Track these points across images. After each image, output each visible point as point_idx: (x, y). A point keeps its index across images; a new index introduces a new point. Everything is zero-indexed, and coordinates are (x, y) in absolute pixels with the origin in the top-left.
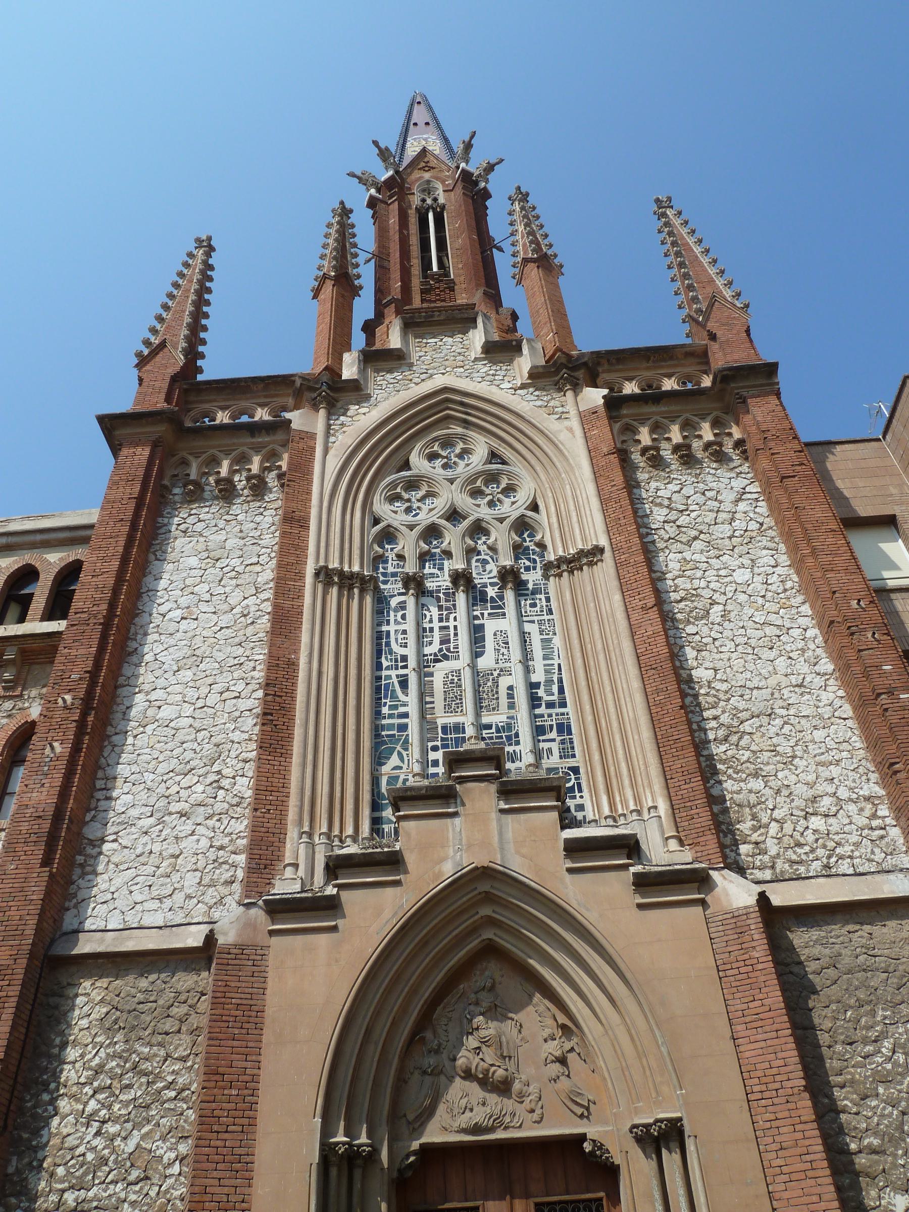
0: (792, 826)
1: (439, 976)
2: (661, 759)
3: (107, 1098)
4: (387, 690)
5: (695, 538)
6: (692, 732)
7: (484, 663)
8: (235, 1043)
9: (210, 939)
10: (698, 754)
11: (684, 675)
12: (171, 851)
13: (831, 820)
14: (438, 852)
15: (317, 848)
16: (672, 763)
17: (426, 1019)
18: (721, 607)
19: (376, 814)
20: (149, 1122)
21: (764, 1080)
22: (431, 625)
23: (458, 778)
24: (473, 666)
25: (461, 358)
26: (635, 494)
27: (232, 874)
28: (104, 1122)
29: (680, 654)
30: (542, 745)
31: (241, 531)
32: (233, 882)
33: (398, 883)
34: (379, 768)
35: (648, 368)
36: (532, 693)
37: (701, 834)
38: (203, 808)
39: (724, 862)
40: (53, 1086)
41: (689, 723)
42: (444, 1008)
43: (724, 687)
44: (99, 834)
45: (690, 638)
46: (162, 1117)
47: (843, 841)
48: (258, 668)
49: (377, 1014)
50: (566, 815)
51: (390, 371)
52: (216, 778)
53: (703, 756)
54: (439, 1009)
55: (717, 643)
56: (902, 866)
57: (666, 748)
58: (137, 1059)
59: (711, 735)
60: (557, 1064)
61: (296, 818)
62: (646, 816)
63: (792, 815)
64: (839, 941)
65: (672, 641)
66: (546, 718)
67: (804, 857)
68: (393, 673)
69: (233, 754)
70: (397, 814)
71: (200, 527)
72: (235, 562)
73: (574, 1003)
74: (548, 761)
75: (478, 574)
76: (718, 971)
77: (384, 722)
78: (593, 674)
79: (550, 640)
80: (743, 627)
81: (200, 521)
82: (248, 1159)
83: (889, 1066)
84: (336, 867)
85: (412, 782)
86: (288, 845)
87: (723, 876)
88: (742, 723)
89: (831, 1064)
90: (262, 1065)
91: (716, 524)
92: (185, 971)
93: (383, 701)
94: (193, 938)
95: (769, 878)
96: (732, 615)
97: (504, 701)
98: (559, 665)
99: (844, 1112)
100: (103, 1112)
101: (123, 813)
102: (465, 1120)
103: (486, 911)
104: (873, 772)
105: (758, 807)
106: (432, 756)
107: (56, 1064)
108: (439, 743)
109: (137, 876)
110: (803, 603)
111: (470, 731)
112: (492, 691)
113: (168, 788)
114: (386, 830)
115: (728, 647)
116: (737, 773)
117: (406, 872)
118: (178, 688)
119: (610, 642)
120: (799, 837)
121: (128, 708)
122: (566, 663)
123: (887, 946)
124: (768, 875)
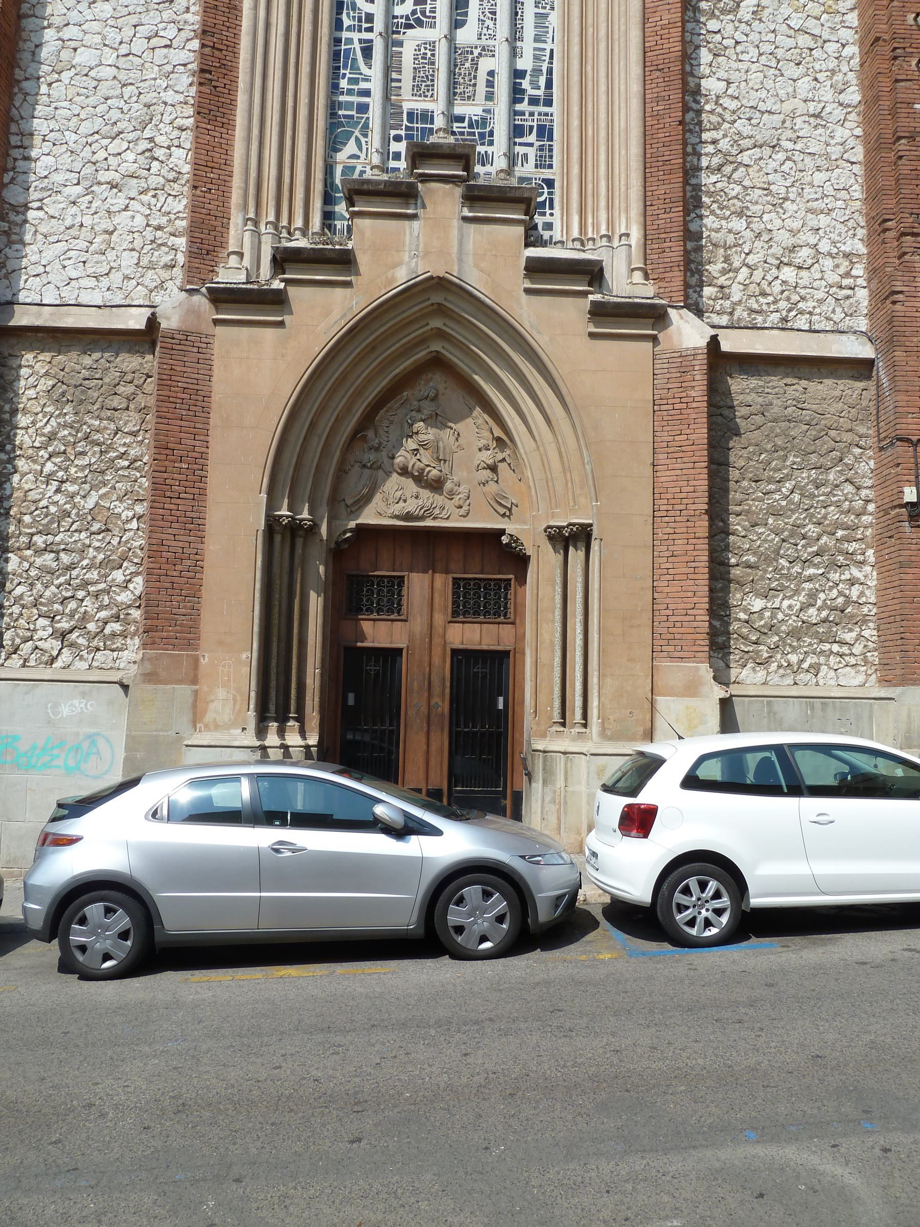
0: (763, 273)
1: (384, 382)
2: (645, 182)
3: (63, 461)
4: (347, 57)
6: (685, 154)
7: (466, 36)
8: (183, 423)
9: (152, 322)
10: (686, 182)
11: (692, 85)
12: (103, 226)
13: (804, 273)
14: (396, 254)
15: (264, 238)
16: (655, 188)
17: (368, 419)
19: (329, 208)
20: (105, 485)
21: (672, 501)
23: (421, 175)
24: (451, 39)
27: (172, 257)
28: (62, 482)
29: (694, 56)
30: (518, 149)
32: (174, 266)
33: (348, 284)
34: (333, 154)
36: (515, 83)
37: (668, 269)
39: (685, 301)
40: (8, 447)
41: (685, 143)
42: (387, 411)
43: (732, 105)
44: (21, 200)
45: (709, 37)
46: (117, 482)
47: (808, 296)
49: (322, 409)
50: (533, 232)
52: (149, 146)
53: (690, 185)
54: (382, 412)
55: (739, 48)
56: (857, 329)
57: (652, 170)
58: (88, 431)
59: (704, 162)
60: (488, 471)
61: (241, 201)
62: (616, 243)
63: (765, 262)
64: (774, 391)
65: (688, 37)
66: (527, 116)
67: (765, 307)
68: (356, 36)
69: (167, 119)
70: (351, 209)
73: (512, 419)
74: (522, 169)
76: (654, 405)
77: (342, 98)
78: (589, 68)
79: (545, 16)
80: (774, 31)
82: (200, 521)
83: (784, 503)
84: (284, 260)
85: (369, 175)
86: (232, 232)
87: (680, 315)
88: (741, 152)
89: (734, 496)
90: (210, 444)
92: (129, 352)
93: (342, 71)
94: (136, 320)
95: (724, 324)
96: (766, 12)
97: (482, 89)
98: (552, 51)
99: (733, 534)
100: (60, 474)
101: (46, 177)
102: (398, 509)
103: (436, 323)
104: (862, 227)
105: (734, 250)
106: (395, 147)
107: (9, 428)
109: (69, 250)
110: (852, 9)
111: (439, 122)
112: (469, 74)
113: (94, 153)
114: (338, 227)
115: (750, 55)
116: (722, 209)
117: (358, 273)
118: (96, 27)
119: (616, 27)
120: (766, 287)
121: (37, 46)
122: (561, 48)
123: (817, 402)
124: (724, 320)
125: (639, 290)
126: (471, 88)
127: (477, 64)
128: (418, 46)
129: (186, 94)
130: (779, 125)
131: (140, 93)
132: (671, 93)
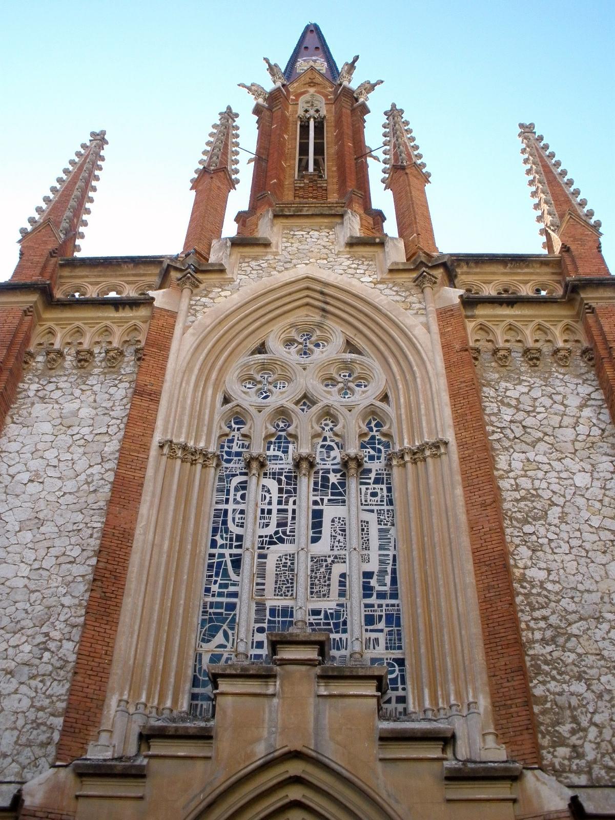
5: (540, 440)
11: (517, 574)
18: (559, 509)
22: (270, 507)
25: (325, 251)
26: (484, 392)
27: (49, 735)
31: (95, 401)
35: (504, 274)
38: (27, 668)
43: (557, 587)
48: (95, 535)
51: (255, 258)
52: (44, 640)
53: (528, 655)
55: (553, 545)
68: (227, 552)
69: (62, 618)
70: (214, 692)
71: (57, 394)
72: (85, 430)
75: (323, 460)
79: (388, 531)
80: (579, 530)
81: (57, 388)
91: (560, 427)
96: (570, 516)
108: (265, 625)
118: (17, 548)
124: (583, 780)
125: (495, 753)
126: (326, 588)
127: (331, 569)
128: (280, 557)
129: (81, 598)
130: (599, 601)
131: (44, 598)
132: (499, 582)
